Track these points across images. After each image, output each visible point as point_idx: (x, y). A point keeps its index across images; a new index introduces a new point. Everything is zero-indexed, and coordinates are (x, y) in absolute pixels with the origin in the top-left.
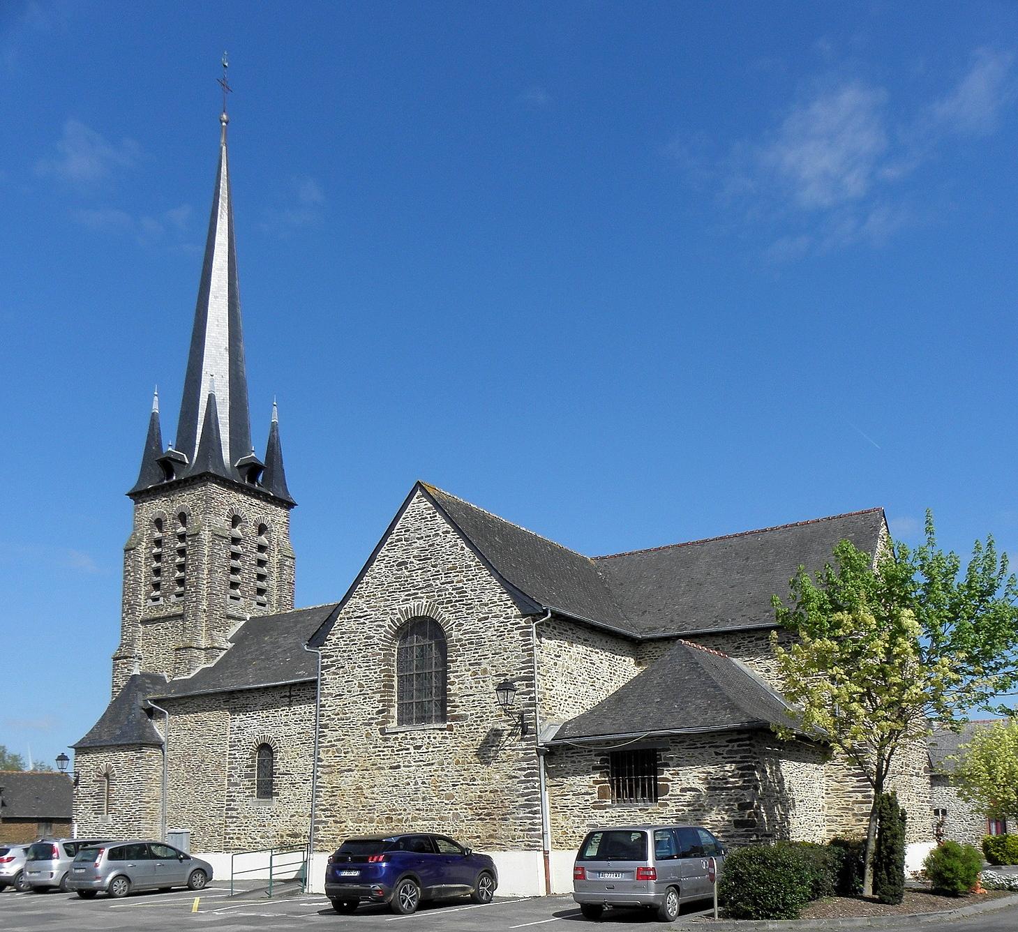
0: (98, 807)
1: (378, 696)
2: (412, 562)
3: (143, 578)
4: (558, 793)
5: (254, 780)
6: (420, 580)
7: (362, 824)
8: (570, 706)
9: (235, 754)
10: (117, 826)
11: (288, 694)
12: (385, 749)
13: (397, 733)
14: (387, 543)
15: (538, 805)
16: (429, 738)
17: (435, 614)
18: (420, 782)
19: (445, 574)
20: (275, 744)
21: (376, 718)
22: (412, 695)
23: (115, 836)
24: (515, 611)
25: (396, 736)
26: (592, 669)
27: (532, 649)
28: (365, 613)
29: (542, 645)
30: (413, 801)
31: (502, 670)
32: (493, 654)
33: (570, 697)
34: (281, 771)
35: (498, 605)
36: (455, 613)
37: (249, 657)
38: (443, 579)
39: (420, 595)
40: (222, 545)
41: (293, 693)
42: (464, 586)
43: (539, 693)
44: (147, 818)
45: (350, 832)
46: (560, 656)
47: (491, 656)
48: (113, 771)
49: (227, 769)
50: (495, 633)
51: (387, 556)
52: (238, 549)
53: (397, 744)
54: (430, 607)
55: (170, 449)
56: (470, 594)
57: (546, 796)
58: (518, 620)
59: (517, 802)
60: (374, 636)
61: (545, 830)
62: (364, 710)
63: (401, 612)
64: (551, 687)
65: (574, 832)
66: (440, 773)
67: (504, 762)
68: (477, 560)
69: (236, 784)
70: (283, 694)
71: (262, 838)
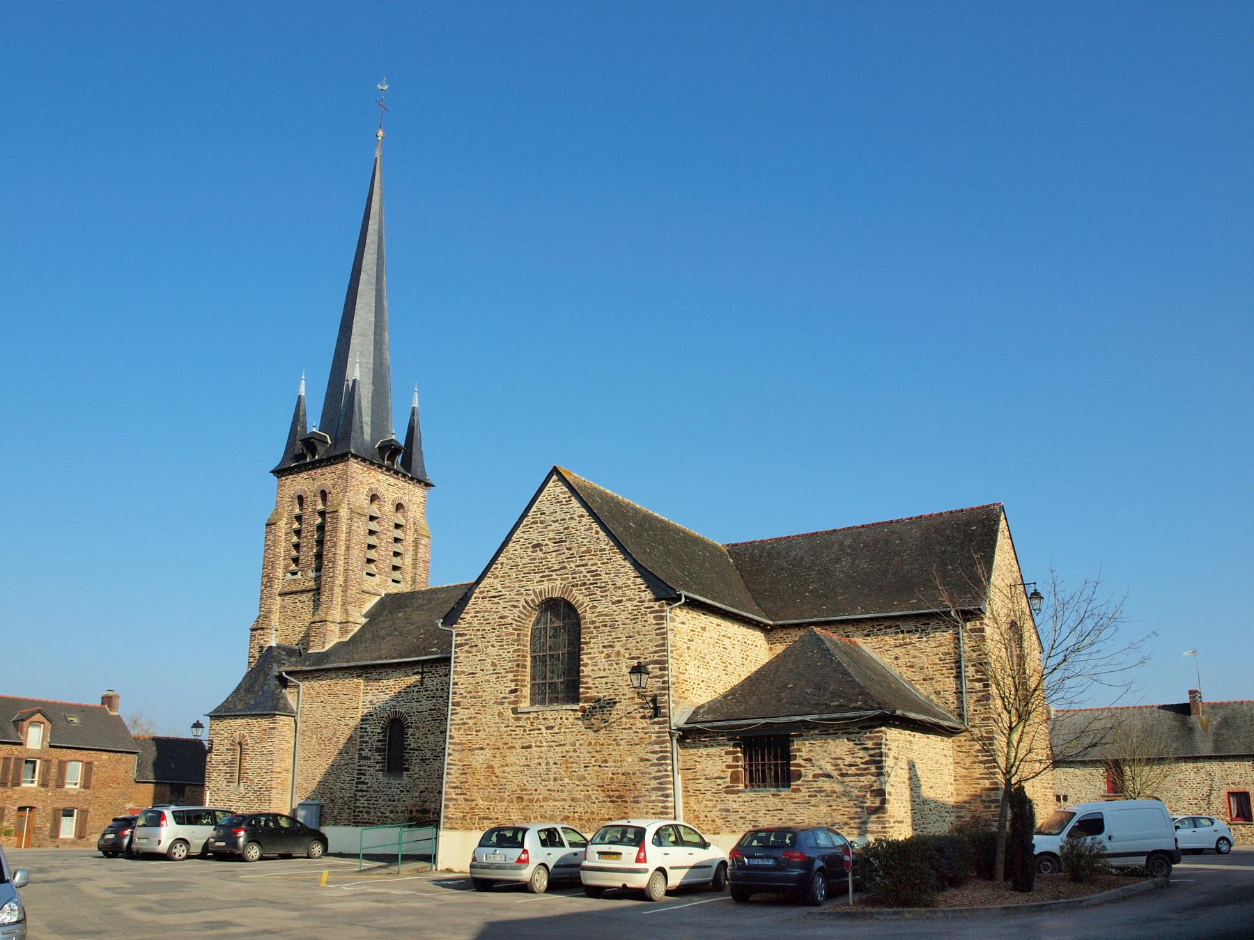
0: (230, 776)
1: (510, 676)
2: (547, 545)
3: (282, 553)
4: (690, 777)
5: (385, 755)
6: (554, 562)
7: (493, 803)
9: (366, 728)
10: (248, 795)
11: (420, 670)
12: (517, 729)
13: (529, 713)
14: (522, 525)
15: (670, 789)
16: (561, 718)
18: (551, 762)
19: (580, 557)
20: (407, 720)
21: (509, 698)
22: (546, 676)
24: (648, 595)
27: (665, 633)
28: (500, 594)
29: (675, 629)
30: (544, 781)
31: (635, 653)
33: (703, 681)
34: (412, 747)
37: (383, 632)
39: (554, 577)
41: (425, 670)
42: (599, 569)
46: (692, 641)
47: (624, 638)
49: (358, 742)
50: (629, 616)
51: (522, 538)
52: (373, 526)
53: (529, 724)
54: (565, 589)
55: (314, 430)
56: (604, 577)
57: (679, 779)
58: (652, 604)
59: (649, 784)
60: (508, 617)
61: (677, 813)
63: (535, 593)
64: (685, 671)
65: (706, 817)
66: (572, 754)
67: (637, 744)
68: (612, 544)
69: (366, 758)
70: (415, 671)
71: (391, 812)
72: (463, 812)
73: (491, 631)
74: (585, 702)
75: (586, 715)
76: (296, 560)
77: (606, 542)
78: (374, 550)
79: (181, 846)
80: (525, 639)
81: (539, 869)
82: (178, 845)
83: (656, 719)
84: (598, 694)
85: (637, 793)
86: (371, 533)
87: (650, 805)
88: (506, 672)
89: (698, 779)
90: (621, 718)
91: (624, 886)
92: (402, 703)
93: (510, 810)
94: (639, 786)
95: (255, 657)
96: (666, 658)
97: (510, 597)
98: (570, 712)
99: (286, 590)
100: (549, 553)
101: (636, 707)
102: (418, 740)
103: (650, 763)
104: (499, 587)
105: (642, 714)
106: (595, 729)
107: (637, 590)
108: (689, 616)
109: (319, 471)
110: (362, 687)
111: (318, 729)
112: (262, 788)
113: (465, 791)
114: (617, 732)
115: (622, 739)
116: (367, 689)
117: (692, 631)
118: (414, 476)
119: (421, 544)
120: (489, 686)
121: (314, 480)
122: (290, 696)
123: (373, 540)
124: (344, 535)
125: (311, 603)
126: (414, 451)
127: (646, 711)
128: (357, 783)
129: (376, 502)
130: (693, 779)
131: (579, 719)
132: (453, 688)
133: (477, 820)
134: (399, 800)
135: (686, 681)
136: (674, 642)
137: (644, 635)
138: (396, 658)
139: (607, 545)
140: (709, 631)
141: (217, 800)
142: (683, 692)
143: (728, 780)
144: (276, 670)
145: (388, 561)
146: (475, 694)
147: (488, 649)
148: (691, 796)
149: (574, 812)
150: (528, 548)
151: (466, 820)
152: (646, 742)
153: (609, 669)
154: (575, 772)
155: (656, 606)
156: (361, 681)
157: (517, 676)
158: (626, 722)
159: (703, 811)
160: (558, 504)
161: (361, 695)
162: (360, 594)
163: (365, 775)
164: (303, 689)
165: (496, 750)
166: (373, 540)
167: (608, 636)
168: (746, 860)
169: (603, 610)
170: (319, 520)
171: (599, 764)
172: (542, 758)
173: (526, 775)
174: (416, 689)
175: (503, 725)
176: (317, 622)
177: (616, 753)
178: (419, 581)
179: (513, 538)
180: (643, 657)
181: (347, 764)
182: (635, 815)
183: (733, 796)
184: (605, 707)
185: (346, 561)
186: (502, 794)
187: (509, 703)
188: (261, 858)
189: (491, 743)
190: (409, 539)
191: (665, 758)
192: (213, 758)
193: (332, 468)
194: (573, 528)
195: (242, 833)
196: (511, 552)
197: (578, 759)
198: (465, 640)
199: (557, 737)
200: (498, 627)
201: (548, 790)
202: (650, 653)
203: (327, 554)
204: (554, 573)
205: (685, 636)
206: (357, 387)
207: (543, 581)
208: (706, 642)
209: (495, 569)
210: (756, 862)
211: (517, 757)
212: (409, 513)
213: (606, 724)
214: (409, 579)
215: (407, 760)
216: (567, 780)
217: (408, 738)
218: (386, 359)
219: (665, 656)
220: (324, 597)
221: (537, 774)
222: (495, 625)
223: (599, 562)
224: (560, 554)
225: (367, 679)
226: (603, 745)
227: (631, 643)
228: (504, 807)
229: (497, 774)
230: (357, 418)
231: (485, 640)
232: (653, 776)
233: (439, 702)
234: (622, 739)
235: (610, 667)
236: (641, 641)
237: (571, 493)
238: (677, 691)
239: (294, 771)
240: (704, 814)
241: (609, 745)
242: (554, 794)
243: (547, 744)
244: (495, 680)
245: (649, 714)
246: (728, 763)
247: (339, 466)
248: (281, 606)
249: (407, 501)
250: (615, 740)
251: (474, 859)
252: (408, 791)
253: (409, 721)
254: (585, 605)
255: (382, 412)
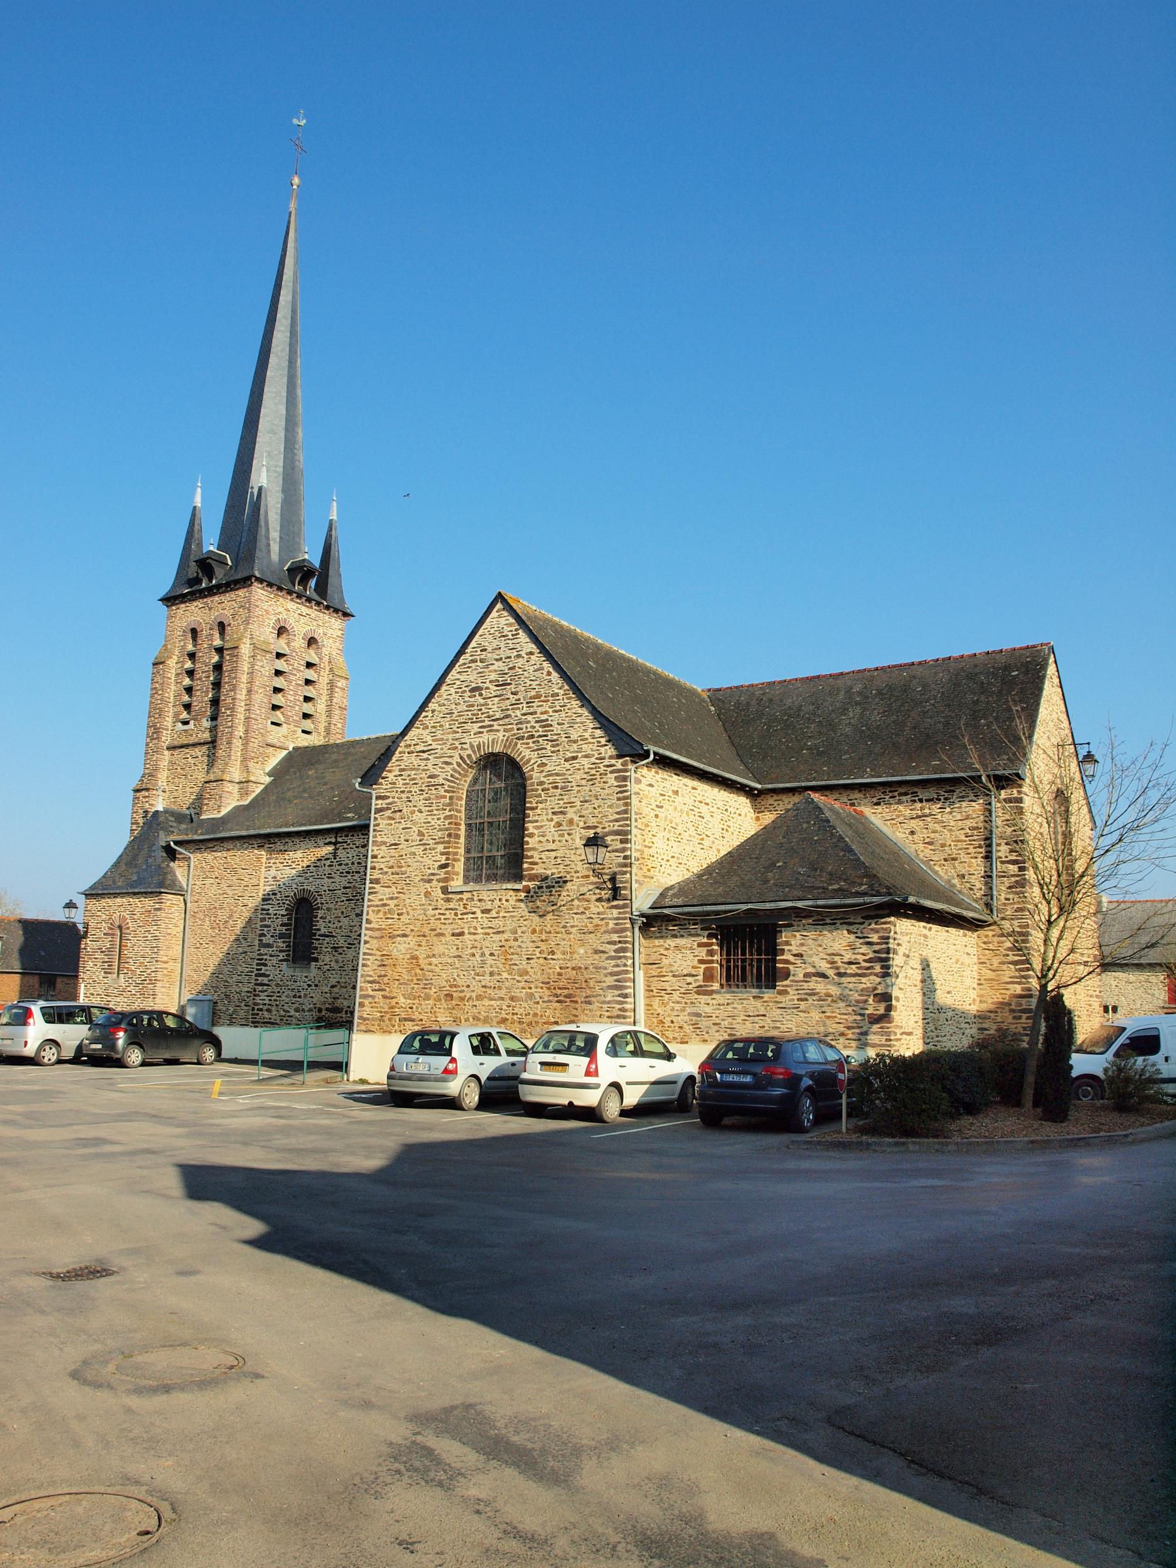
0: (109, 966)
1: (440, 848)
2: (487, 688)
3: (172, 698)
4: (654, 974)
5: (290, 942)
6: (496, 709)
7: (416, 1001)
8: (673, 868)
9: (269, 910)
10: (129, 989)
11: (333, 840)
12: (447, 912)
13: (462, 892)
14: (458, 664)
15: (630, 987)
16: (500, 900)
17: (513, 750)
18: (487, 953)
19: (527, 703)
20: (316, 899)
21: (438, 874)
22: (482, 848)
23: (126, 1000)
24: (610, 750)
25: (461, 896)
26: (700, 823)
27: (629, 797)
28: (430, 747)
30: (478, 975)
31: (592, 821)
32: (581, 802)
33: (673, 857)
34: (322, 932)
35: (590, 743)
36: (537, 750)
38: (525, 709)
39: (496, 727)
40: (265, 661)
41: (339, 840)
42: (550, 719)
43: (637, 850)
44: (163, 981)
45: (402, 1009)
46: (662, 807)
48: (128, 923)
49: (258, 926)
50: (585, 776)
51: (458, 679)
52: (281, 665)
53: (462, 906)
54: (508, 743)
55: (212, 548)
56: (556, 729)
58: (613, 762)
59: (604, 982)
60: (439, 775)
61: (637, 1017)
62: (423, 864)
63: (472, 746)
65: (672, 1022)
66: (512, 943)
67: (591, 933)
68: (566, 687)
69: (268, 946)
70: (328, 840)
71: (297, 1010)
72: (381, 1012)
73: (418, 793)
74: (530, 880)
75: (530, 895)
76: (187, 707)
77: (560, 685)
78: (281, 694)
79: (51, 1048)
80: (460, 802)
81: (469, 1082)
82: (47, 1048)
83: (615, 903)
84: (545, 871)
85: (589, 992)
86: (278, 673)
87: (605, 1006)
88: (436, 843)
89: (664, 976)
90: (572, 900)
91: (571, 1103)
92: (311, 879)
93: (437, 1010)
94: (592, 983)
95: (139, 824)
96: (629, 828)
97: (442, 752)
98: (511, 893)
99: (176, 743)
100: (490, 698)
101: (591, 887)
102: (329, 925)
103: (607, 955)
104: (429, 739)
105: (598, 896)
106: (541, 914)
107: (595, 745)
108: (658, 777)
109: (216, 598)
110: (264, 860)
111: (212, 910)
112: (146, 980)
113: (383, 987)
114: (567, 917)
115: (572, 927)
116: (269, 863)
117: (662, 795)
118: (331, 605)
119: (337, 687)
120: (415, 860)
121: (210, 609)
122: (179, 870)
123: (279, 682)
124: (245, 676)
125: (205, 759)
126: (330, 574)
127: (603, 892)
128: (257, 975)
129: (284, 636)
130: (658, 976)
131: (521, 900)
132: (372, 862)
133: (398, 1021)
134: (305, 995)
135: (653, 856)
136: (639, 809)
137: (603, 799)
138: (305, 825)
139: (560, 688)
140: (683, 796)
141: (93, 994)
142: (649, 870)
143: (701, 978)
144: (163, 839)
145: (297, 708)
146: (397, 869)
147: (414, 815)
148: (654, 996)
149: (513, 1013)
150: (465, 692)
151: (383, 1021)
152: (602, 931)
153: (559, 841)
154: (516, 965)
155: (618, 764)
156: (263, 853)
157: (449, 848)
158: (578, 905)
159: (669, 1016)
160: (503, 639)
161: (263, 869)
162: (263, 747)
163: (265, 965)
164: (195, 862)
165: (421, 938)
166: (279, 682)
167: (559, 800)
168: (718, 1075)
169: (554, 768)
170: (216, 658)
171: (544, 956)
172: (476, 947)
173: (457, 968)
174: (328, 863)
175: (430, 908)
176: (211, 782)
177: (565, 942)
178: (334, 732)
179: (447, 680)
180: (601, 826)
181: (246, 952)
182: (586, 1019)
183: (706, 997)
184: (553, 887)
185: (247, 707)
186: (427, 991)
187: (439, 880)
188: (144, 1064)
189: (416, 929)
190: (323, 680)
191: (624, 950)
192: (88, 945)
193: (232, 595)
194: (520, 668)
195: (121, 1034)
196: (445, 697)
197: (519, 949)
198: (387, 804)
199: (495, 923)
200: (427, 788)
201: (483, 987)
202: (610, 821)
203: (226, 700)
204: (495, 723)
205: (652, 801)
206: (263, 495)
207: (482, 733)
208: (679, 809)
209: (424, 717)
210: (730, 1078)
211: (446, 946)
212: (324, 649)
213: (555, 907)
214: (322, 729)
215: (316, 948)
216: (505, 975)
217: (318, 921)
218: (299, 461)
219: (627, 825)
220: (220, 751)
221: (469, 967)
222: (423, 785)
223: (550, 710)
224: (503, 700)
225: (270, 851)
226: (550, 932)
227: (587, 809)
228: (429, 1007)
229: (423, 966)
230: (263, 534)
231: (410, 804)
232: (609, 971)
233: (354, 878)
234: (572, 927)
235: (561, 838)
236: (599, 807)
237: (519, 625)
238: (641, 869)
239: (182, 960)
240: (669, 1019)
241: (557, 933)
242: (489, 991)
243: (483, 931)
244: (422, 853)
245: (607, 896)
246: (701, 958)
247: (241, 592)
248: (171, 762)
249: (322, 635)
250: (564, 927)
251: (392, 1069)
252: (316, 986)
253: (319, 901)
254: (532, 761)
255: (294, 526)
